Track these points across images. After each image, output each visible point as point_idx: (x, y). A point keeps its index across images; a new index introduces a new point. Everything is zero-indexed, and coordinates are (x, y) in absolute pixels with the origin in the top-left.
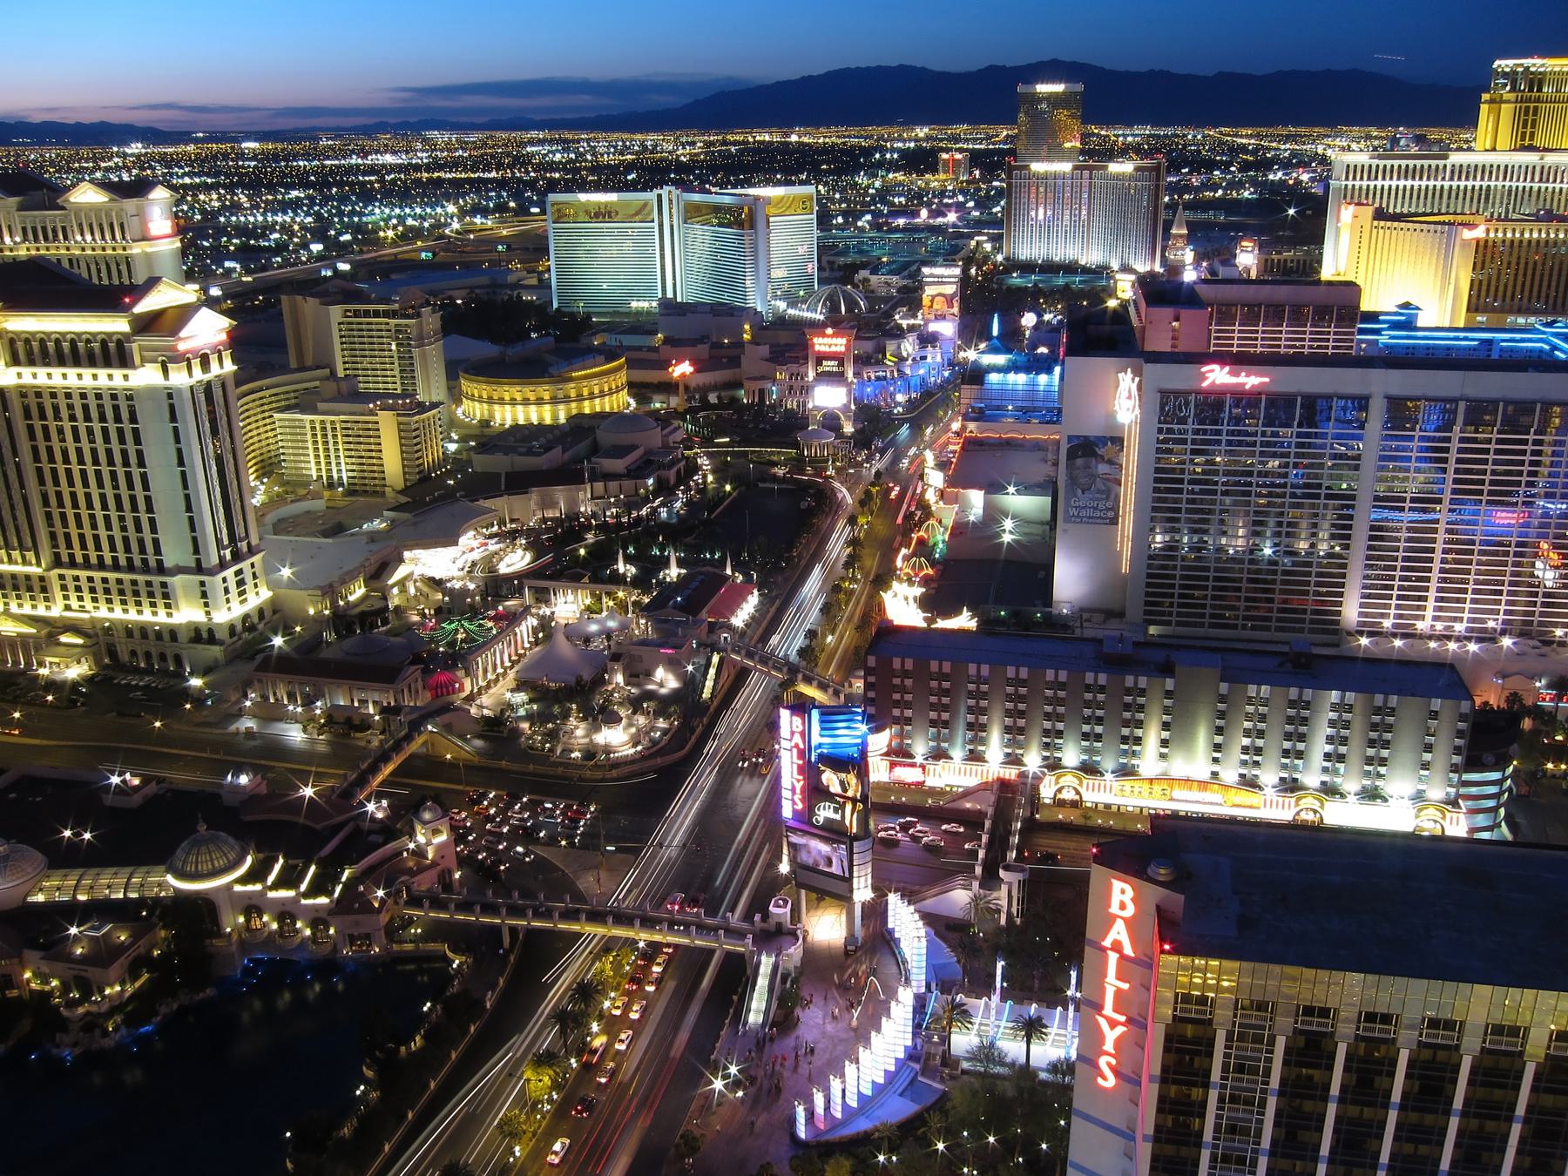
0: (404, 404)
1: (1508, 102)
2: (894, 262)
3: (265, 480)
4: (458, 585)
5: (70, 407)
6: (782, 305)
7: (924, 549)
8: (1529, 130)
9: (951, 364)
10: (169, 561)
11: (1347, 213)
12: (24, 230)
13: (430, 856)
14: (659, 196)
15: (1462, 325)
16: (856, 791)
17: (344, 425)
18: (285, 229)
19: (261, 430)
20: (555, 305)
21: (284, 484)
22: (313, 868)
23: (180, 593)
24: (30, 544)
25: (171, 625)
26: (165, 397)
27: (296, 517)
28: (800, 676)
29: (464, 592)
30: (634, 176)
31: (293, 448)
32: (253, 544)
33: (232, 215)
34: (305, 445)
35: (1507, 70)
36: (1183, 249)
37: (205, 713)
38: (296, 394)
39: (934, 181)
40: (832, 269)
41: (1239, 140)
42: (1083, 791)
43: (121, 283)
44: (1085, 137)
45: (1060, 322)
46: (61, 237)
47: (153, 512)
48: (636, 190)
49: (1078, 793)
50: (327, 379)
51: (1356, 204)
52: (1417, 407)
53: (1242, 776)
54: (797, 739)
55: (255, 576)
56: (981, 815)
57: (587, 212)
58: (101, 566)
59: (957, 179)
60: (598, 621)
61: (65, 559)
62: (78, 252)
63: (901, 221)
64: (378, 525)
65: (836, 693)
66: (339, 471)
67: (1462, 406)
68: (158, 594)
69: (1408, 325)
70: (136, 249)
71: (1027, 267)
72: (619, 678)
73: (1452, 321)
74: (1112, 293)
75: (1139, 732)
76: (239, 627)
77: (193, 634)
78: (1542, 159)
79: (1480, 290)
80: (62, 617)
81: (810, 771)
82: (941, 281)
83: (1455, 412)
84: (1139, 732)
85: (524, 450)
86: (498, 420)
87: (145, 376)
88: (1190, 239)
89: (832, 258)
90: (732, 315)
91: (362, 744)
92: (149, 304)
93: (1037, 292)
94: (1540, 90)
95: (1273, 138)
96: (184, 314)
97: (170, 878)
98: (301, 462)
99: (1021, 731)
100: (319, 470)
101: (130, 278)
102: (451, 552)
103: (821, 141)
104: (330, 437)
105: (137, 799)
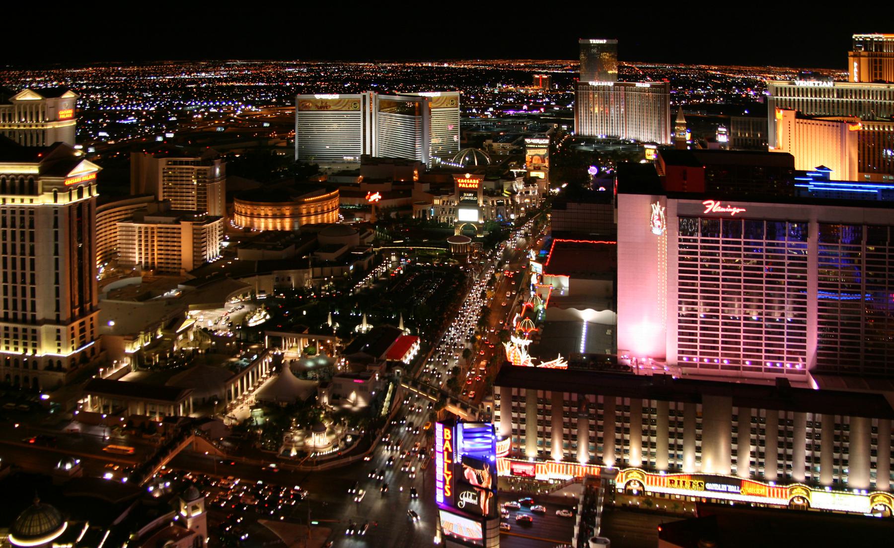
0: (198, 217)
1: (864, 56)
2: (507, 135)
3: (106, 264)
7: (531, 313)
9: (544, 195)
10: (39, 316)
11: (780, 115)
13: (189, 526)
14: (364, 97)
15: (856, 180)
16: (488, 483)
17: (159, 230)
18: (138, 114)
19: (108, 233)
21: (117, 266)
22: (108, 532)
23: (43, 337)
26: (53, 213)
27: (122, 288)
28: (448, 400)
29: (226, 338)
31: (126, 244)
35: (861, 40)
36: (684, 131)
39: (531, 90)
40: (469, 139)
42: (645, 484)
43: (38, 145)
44: (620, 68)
49: (641, 485)
53: (752, 473)
54: (447, 444)
56: (575, 501)
59: (544, 89)
60: (312, 360)
62: (16, 128)
63: (511, 112)
64: (174, 293)
65: (473, 412)
67: (865, 229)
68: (30, 338)
69: (825, 178)
70: (50, 126)
71: (590, 140)
72: (325, 400)
73: (850, 176)
74: (644, 158)
76: (78, 360)
77: (47, 364)
78: (889, 87)
81: (456, 470)
83: (861, 232)
85: (271, 247)
87: (44, 200)
88: (688, 126)
89: (469, 133)
90: (407, 165)
94: (881, 50)
95: (731, 71)
97: (11, 538)
99: (600, 440)
101: (43, 142)
102: (219, 312)
103: (462, 66)
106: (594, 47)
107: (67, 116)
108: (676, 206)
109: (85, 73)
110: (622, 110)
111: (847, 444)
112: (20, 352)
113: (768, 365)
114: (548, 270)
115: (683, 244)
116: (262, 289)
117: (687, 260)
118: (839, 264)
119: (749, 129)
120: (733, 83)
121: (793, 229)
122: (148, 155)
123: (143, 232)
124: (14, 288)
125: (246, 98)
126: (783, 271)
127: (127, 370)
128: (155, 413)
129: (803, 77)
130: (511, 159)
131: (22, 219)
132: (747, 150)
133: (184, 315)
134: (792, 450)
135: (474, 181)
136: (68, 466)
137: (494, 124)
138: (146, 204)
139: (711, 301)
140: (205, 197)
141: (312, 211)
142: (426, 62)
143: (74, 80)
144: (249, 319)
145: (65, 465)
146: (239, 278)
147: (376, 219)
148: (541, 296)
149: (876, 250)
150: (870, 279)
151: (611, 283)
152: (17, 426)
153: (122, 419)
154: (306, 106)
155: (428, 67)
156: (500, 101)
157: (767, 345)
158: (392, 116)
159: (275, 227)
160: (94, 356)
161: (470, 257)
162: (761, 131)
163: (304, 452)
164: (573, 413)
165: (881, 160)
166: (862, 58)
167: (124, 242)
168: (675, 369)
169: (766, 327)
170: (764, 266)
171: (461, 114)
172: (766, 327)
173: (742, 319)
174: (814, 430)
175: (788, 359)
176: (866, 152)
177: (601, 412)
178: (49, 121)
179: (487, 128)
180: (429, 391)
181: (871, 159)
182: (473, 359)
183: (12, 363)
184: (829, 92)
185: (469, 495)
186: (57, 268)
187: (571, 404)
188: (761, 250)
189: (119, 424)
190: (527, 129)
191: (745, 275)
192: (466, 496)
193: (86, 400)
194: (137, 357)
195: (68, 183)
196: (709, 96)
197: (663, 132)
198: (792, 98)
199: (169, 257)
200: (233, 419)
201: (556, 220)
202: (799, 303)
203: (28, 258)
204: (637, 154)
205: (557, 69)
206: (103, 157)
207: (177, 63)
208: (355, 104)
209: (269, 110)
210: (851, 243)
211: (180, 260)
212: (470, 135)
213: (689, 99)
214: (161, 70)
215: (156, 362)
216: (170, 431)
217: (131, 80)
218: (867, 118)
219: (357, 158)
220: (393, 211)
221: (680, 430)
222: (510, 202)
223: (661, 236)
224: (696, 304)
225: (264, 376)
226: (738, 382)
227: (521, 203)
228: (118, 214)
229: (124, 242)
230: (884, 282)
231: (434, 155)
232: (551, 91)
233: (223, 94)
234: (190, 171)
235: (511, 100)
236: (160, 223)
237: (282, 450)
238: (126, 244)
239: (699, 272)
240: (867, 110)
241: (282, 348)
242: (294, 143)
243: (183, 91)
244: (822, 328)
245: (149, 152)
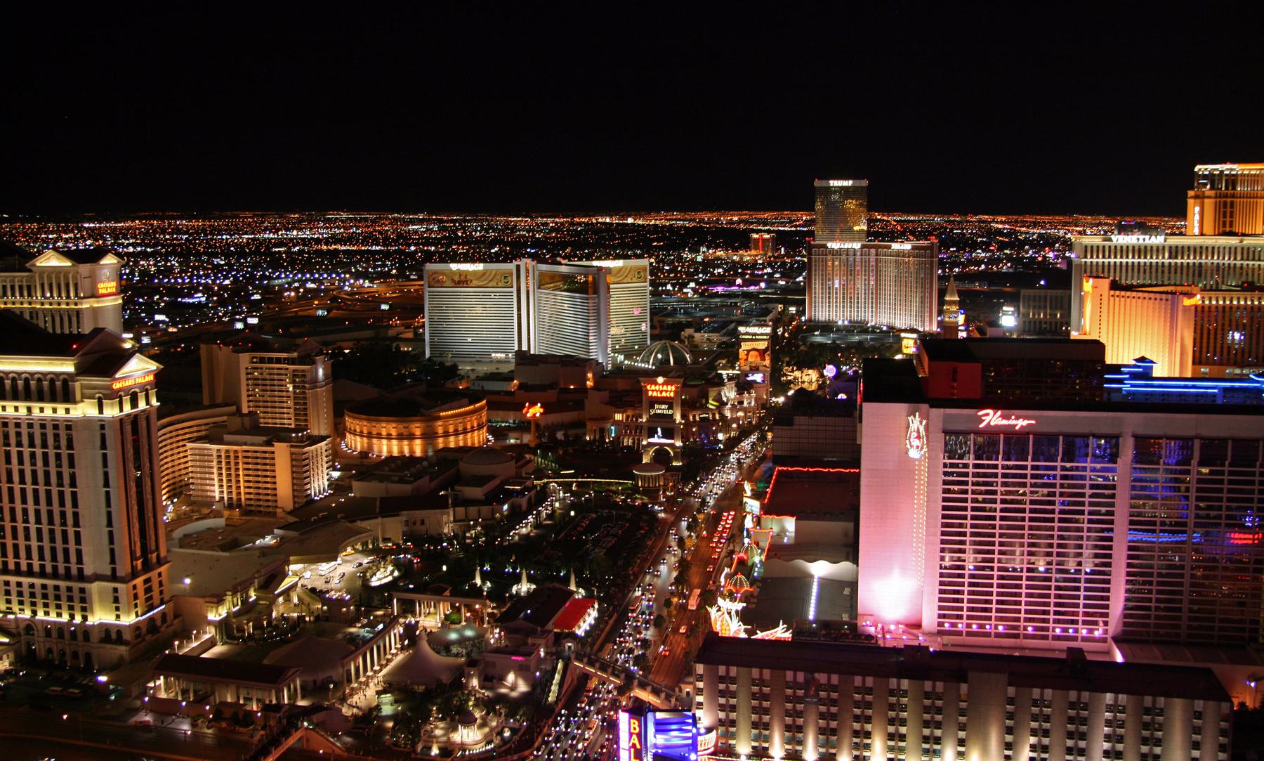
0: (297, 437)
1: (1209, 197)
2: (714, 322)
3: (175, 500)
5: (19, 434)
7: (744, 567)
8: (1228, 219)
10: (88, 570)
11: (1088, 285)
14: (518, 267)
15: (1189, 375)
19: (176, 457)
20: (428, 355)
23: (95, 598)
26: (98, 428)
27: (199, 533)
28: (636, 682)
29: (340, 602)
30: (496, 249)
31: (200, 473)
35: (1206, 173)
36: (955, 312)
37: (108, 707)
39: (747, 256)
40: (662, 327)
41: (996, 225)
43: (71, 332)
44: (871, 222)
45: (856, 372)
47: (79, 527)
48: (498, 261)
50: (233, 414)
52: (1160, 444)
54: (635, 740)
58: (30, 573)
59: (765, 255)
60: (457, 631)
62: (38, 306)
63: (720, 289)
64: (269, 540)
65: (668, 698)
67: (1197, 443)
68: (77, 599)
69: (1146, 375)
70: (86, 305)
71: (827, 327)
72: (475, 682)
74: (900, 351)
76: (144, 630)
78: (1241, 242)
79: (1201, 347)
82: (756, 336)
87: (85, 410)
88: (962, 305)
90: (578, 365)
91: (245, 738)
93: (834, 348)
94: (1234, 188)
95: (1024, 224)
99: (834, 732)
101: (78, 328)
103: (653, 222)
104: (232, 464)
106: (835, 192)
107: (109, 291)
108: (941, 419)
109: (130, 228)
110: (872, 283)
111: (1160, 733)
112: (65, 618)
113: (1058, 631)
114: (768, 510)
115: (950, 470)
116: (388, 537)
117: (954, 492)
118: (1159, 494)
119: (1045, 307)
120: (1026, 242)
121: (1099, 446)
122: (224, 348)
123: (223, 456)
124: (52, 532)
125: (355, 268)
126: (1082, 504)
127: (211, 643)
128: (251, 699)
129: (1123, 230)
130: (720, 356)
131: (57, 437)
132: (1042, 337)
133: (284, 569)
134: (1085, 742)
135: (669, 388)
137: (697, 306)
138: (225, 418)
139: (984, 548)
140: (306, 409)
141: (451, 429)
142: (602, 216)
143: (116, 238)
144: (372, 577)
146: (355, 521)
147: (537, 441)
148: (757, 544)
149: (1211, 473)
150: (1201, 512)
151: (851, 525)
152: (65, 717)
153: (208, 708)
154: (439, 281)
155: (604, 224)
156: (705, 273)
157: (1057, 605)
158: (556, 295)
159: (401, 451)
160: (166, 625)
161: (664, 493)
162: (1061, 308)
163: (447, 750)
165: (1225, 346)
166: (1206, 201)
167: (198, 469)
168: (932, 639)
169: (1056, 581)
170: (1057, 499)
171: (651, 291)
172: (1056, 581)
173: (1025, 570)
174: (1115, 716)
175: (1085, 623)
176: (1205, 336)
177: (834, 695)
178: (84, 298)
179: (686, 313)
181: (1212, 345)
182: (667, 628)
183: (54, 634)
184: (1158, 250)
186: (108, 504)
187: (795, 685)
188: (1054, 477)
189: (203, 715)
190: (741, 313)
191: (1031, 511)
193: (158, 683)
194: (224, 626)
195: (116, 386)
196: (992, 261)
197: (927, 314)
198: (1106, 261)
199: (261, 491)
200: (354, 707)
201: (780, 440)
202: (1103, 547)
203: (68, 491)
204: (891, 346)
205: (783, 224)
206: (163, 351)
207: (258, 216)
208: (505, 277)
209: (389, 286)
210: (1177, 464)
211: (276, 495)
212: (663, 321)
213: (964, 265)
214: (236, 225)
215: (249, 633)
216: (272, 723)
217: (195, 239)
218: (1208, 287)
219: (510, 355)
220: (560, 430)
221: (938, 717)
222: (717, 417)
223: (920, 460)
224: (963, 551)
225: (394, 651)
226: (1017, 654)
227: (732, 418)
228: (187, 430)
229: (198, 469)
230: (1219, 517)
231: (614, 351)
232: (775, 257)
233: (323, 261)
234: (283, 372)
235: (720, 270)
236: (245, 444)
237: (419, 748)
238: (200, 473)
239: (969, 509)
240: (1209, 275)
241: (416, 614)
242: (424, 333)
243: (266, 256)
244: (1132, 581)
245: (226, 345)
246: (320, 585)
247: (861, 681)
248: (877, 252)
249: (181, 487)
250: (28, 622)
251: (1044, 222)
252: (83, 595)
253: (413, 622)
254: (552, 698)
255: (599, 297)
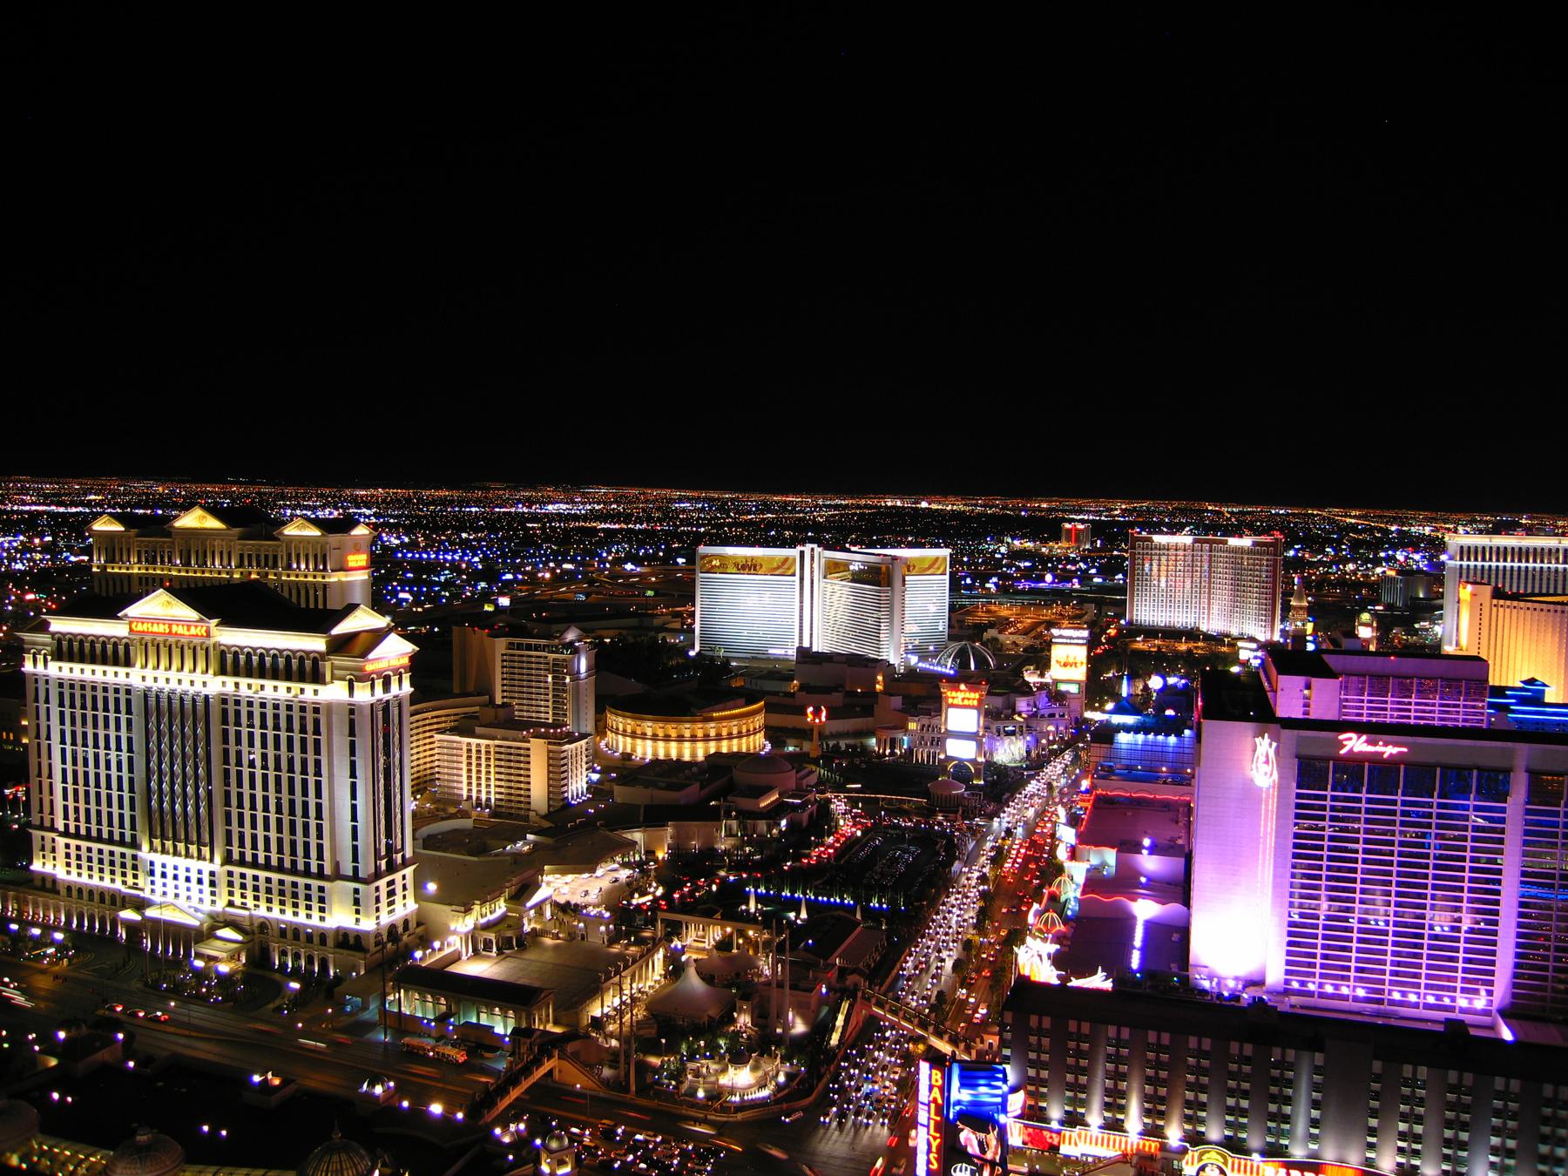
3: (419, 796)
4: (593, 911)
6: (914, 660)
11: (1466, 592)
12: (241, 556)
14: (802, 553)
16: (996, 1153)
17: (498, 749)
18: (455, 567)
19: (421, 749)
21: (435, 801)
24: (207, 840)
25: (323, 928)
27: (444, 834)
32: (407, 856)
33: (409, 552)
34: (459, 759)
38: (457, 717)
39: (1058, 548)
40: (961, 627)
41: (1348, 520)
46: (246, 563)
50: (486, 706)
51: (1472, 583)
54: (936, 1093)
55: (405, 888)
57: (736, 565)
59: (1078, 548)
61: (236, 856)
66: (488, 793)
70: (334, 578)
71: (1151, 632)
75: (1287, 1109)
80: (224, 912)
81: (947, 1130)
84: (1287, 1109)
85: (664, 785)
86: (639, 753)
87: (333, 692)
89: (961, 617)
90: (867, 666)
92: (344, 628)
96: (378, 636)
98: (454, 781)
99: (1162, 1100)
100: (470, 790)
103: (949, 508)
105: (274, 1100)
123: (483, 752)
136: (378, 1090)
141: (724, 733)
145: (374, 1087)
163: (716, 1094)
164: (1121, 1056)
175: (1463, 990)
180: (901, 1014)
185: (966, 1169)
192: (961, 1170)
195: (369, 668)
198: (1486, 564)
211: (529, 796)
212: (963, 621)
238: (448, 768)
246: (576, 899)
247: (1155, 1037)
248: (1211, 547)
249: (426, 782)
250: (262, 920)
251: (1406, 518)
252: (295, 890)
253: (679, 947)
254: (835, 1039)
255: (892, 590)
